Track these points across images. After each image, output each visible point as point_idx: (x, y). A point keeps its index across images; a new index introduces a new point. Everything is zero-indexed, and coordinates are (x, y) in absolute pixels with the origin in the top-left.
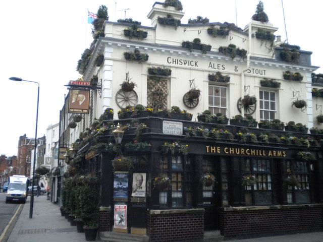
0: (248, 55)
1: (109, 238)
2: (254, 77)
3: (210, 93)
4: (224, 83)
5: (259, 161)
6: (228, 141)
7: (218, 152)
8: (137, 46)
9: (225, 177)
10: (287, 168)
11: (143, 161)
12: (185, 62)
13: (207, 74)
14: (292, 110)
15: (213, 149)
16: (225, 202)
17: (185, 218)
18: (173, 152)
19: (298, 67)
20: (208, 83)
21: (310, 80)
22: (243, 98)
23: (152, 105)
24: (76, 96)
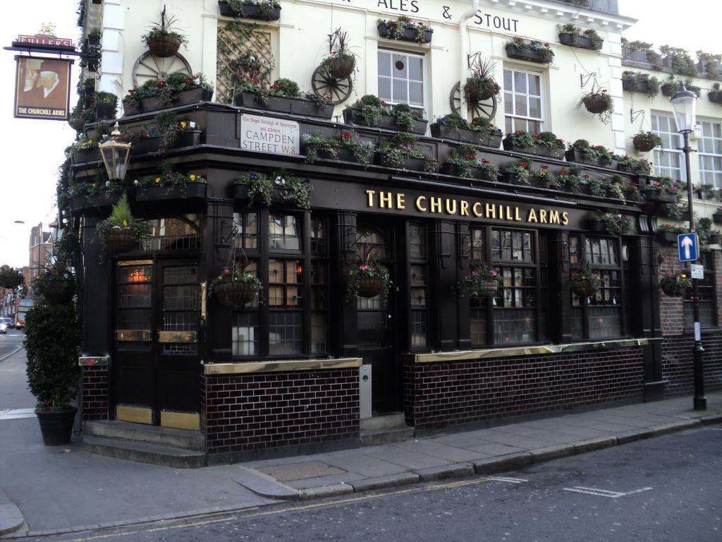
1: (105, 437)
2: (491, 34)
3: (383, 69)
4: (417, 45)
6: (425, 177)
7: (399, 206)
9: (418, 274)
10: (570, 254)
11: (188, 229)
13: (372, 22)
14: (575, 114)
15: (386, 200)
16: (417, 340)
17: (308, 383)
19: (592, 16)
20: (375, 44)
21: (618, 50)
22: (464, 83)
23: (231, 94)
24: (35, 74)
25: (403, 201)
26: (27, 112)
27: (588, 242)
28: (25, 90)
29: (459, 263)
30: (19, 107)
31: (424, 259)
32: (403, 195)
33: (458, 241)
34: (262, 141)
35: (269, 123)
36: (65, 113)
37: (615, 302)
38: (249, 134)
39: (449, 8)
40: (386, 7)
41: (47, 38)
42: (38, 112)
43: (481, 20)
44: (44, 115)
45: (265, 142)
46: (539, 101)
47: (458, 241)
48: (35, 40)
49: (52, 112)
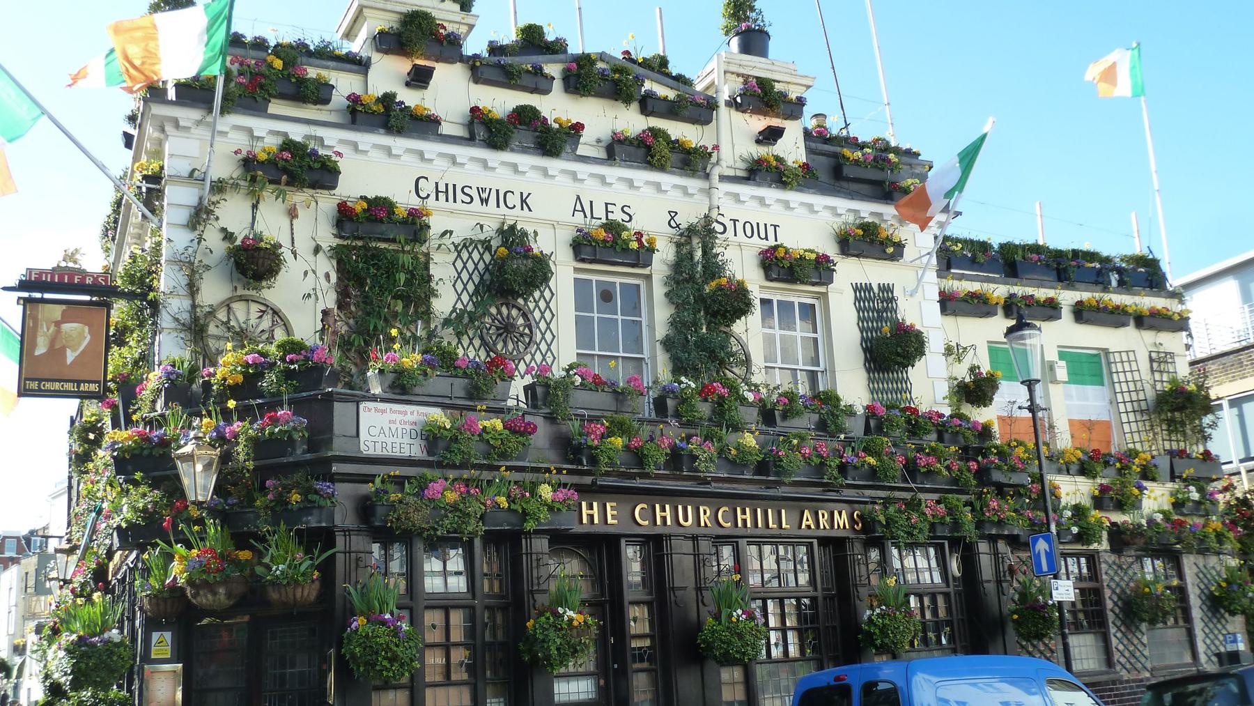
0: (716, 172)
5: (767, 549)
7: (610, 521)
8: (297, 133)
12: (484, 196)
18: (378, 668)
24: (52, 328)
25: (615, 513)
26: (39, 386)
27: (895, 552)
28: (37, 353)
29: (700, 597)
30: (26, 379)
31: (651, 594)
32: (614, 504)
33: (699, 562)
34: (392, 440)
35: (400, 412)
36: (99, 387)
37: (944, 641)
38: (373, 431)
39: (676, 213)
40: (585, 217)
41: (72, 272)
42: (57, 386)
43: (725, 228)
44: (66, 391)
45: (394, 440)
46: (815, 340)
47: (699, 562)
48: (52, 277)
49: (78, 387)
